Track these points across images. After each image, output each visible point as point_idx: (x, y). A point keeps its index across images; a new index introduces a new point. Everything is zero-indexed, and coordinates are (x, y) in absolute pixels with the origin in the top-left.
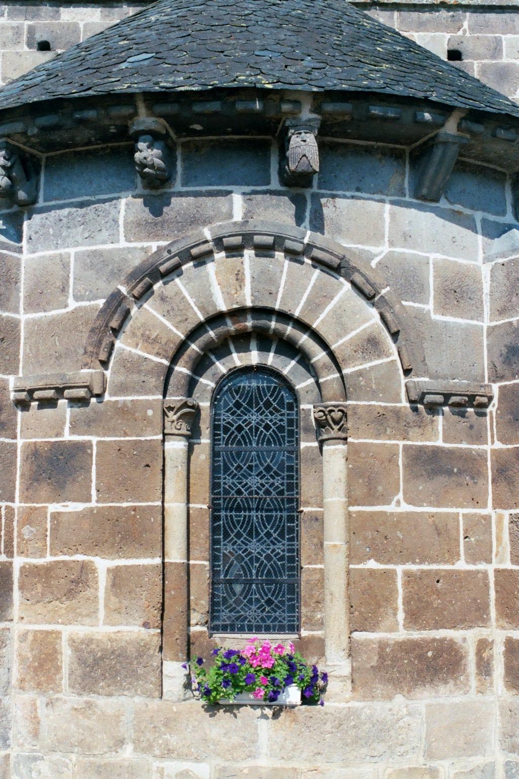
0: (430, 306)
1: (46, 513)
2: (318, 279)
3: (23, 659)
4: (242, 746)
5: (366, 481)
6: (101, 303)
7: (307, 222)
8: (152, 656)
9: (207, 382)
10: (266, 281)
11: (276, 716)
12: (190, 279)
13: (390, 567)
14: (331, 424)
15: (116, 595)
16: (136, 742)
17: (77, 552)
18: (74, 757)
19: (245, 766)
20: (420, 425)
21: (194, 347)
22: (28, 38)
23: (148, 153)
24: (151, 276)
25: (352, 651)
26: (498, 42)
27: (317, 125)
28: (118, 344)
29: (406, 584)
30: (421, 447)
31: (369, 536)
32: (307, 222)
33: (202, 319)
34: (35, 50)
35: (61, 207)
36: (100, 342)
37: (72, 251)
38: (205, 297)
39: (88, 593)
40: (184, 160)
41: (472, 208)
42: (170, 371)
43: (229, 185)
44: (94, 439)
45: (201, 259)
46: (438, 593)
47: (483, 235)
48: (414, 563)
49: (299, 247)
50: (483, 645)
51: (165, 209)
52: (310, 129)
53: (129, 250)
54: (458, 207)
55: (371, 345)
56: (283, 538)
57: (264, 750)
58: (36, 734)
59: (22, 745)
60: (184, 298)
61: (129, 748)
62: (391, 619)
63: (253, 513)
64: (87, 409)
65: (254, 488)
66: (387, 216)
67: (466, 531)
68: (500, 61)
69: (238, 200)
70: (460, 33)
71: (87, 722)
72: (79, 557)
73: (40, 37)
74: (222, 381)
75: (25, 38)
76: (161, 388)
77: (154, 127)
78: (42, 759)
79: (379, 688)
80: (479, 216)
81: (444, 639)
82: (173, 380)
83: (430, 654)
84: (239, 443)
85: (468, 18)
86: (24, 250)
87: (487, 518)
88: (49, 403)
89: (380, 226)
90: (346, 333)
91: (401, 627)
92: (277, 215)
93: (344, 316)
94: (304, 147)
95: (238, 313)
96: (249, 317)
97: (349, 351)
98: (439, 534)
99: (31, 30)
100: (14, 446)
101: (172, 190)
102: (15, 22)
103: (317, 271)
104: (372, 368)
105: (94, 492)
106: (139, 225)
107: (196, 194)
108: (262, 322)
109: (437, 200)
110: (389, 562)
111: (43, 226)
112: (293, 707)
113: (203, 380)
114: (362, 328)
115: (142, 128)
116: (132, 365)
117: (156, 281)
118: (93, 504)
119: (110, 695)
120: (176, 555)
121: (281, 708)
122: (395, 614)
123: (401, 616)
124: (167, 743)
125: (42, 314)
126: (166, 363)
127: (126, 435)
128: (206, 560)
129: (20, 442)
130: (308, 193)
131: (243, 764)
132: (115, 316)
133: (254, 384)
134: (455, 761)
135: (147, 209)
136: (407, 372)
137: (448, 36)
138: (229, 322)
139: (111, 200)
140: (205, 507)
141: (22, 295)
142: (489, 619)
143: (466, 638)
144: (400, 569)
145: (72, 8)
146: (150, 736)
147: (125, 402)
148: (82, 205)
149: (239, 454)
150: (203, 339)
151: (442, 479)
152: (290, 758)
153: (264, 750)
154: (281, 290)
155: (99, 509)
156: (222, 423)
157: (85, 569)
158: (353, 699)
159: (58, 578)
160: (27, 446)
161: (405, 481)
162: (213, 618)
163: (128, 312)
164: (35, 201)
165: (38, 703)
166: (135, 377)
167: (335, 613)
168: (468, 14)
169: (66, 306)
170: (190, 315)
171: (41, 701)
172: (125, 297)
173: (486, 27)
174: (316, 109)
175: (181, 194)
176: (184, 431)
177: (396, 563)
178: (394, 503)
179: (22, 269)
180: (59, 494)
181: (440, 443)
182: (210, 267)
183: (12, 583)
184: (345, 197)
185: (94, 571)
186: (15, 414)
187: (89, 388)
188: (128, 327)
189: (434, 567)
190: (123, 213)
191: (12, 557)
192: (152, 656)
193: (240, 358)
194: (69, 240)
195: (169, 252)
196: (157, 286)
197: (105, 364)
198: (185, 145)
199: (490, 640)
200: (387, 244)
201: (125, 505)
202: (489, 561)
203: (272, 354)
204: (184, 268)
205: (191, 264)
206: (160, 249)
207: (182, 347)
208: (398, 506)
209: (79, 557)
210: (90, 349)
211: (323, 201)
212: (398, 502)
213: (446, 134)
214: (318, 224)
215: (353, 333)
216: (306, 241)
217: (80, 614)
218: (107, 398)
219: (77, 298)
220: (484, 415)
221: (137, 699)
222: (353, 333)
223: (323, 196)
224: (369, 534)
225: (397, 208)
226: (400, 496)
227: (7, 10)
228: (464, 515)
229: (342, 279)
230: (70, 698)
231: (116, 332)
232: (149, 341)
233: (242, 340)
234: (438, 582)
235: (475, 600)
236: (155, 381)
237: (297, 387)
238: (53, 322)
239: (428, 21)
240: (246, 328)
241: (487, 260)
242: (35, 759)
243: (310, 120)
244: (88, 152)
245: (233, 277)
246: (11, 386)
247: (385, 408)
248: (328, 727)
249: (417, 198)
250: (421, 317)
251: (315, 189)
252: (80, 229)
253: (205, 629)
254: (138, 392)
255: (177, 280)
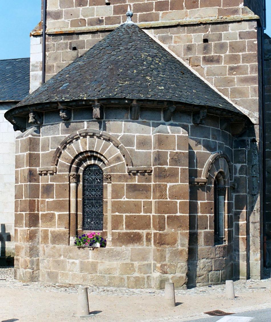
0: (135, 148)
1: (45, 201)
2: (105, 143)
3: (42, 236)
4: (85, 256)
5: (116, 193)
6: (55, 149)
7: (102, 129)
8: (67, 235)
9: (82, 168)
10: (92, 144)
11: (93, 249)
12: (75, 144)
13: (122, 214)
14: (109, 178)
15: (59, 221)
16: (64, 255)
17: (51, 211)
18: (51, 259)
19: (86, 261)
20: (131, 178)
21: (77, 160)
22: (70, 46)
23: (62, 114)
24: (65, 144)
25: (113, 234)
26: (221, 34)
27: (99, 106)
28: (59, 160)
29: (126, 219)
30: (131, 184)
31: (118, 207)
32: (102, 129)
33: (77, 154)
34: (72, 50)
35: (47, 125)
36: (55, 160)
37: (50, 136)
38: (78, 148)
39: (54, 220)
40: (73, 113)
41: (149, 120)
42: (71, 167)
43: (83, 119)
44: (55, 183)
45: (77, 139)
46: (135, 221)
47: (153, 127)
48: (128, 213)
49: (99, 135)
50: (148, 234)
51: (69, 126)
52: (98, 107)
53: (62, 137)
54: (144, 120)
55: (118, 159)
56: (100, 207)
57: (91, 257)
58: (44, 254)
59: (42, 257)
60: (73, 149)
61: (62, 256)
62: (122, 227)
63: (93, 201)
64: (53, 176)
65: (94, 195)
66: (123, 125)
67: (144, 205)
68: (221, 42)
69: (85, 123)
70: (208, 33)
71: (54, 251)
72: (52, 212)
73: (73, 46)
74: (85, 168)
75: (69, 46)
76: (68, 171)
77: (62, 108)
78: (45, 259)
79: (118, 244)
80: (151, 122)
81: (136, 232)
82: (72, 168)
83: (132, 236)
84: (90, 183)
85: (210, 27)
86: (41, 136)
87: (151, 201)
88: (46, 174)
89: (122, 128)
90: (112, 156)
91: (124, 229)
92: (95, 127)
93: (110, 152)
94: (97, 111)
95: (86, 152)
96: (89, 153)
97: (112, 161)
98: (135, 206)
99: (70, 43)
100: (39, 185)
101: (71, 121)
102: (66, 41)
103: (104, 141)
104: (118, 164)
105: (55, 196)
106: (64, 130)
107: (76, 122)
108: (92, 154)
109: (138, 119)
110: (121, 213)
111: (44, 130)
112: (97, 248)
113: (81, 168)
114: (116, 154)
115: (60, 108)
116: (62, 165)
117: (67, 144)
118: (55, 199)
119: (58, 244)
120: (73, 211)
121: (95, 248)
122: (123, 226)
123: (124, 226)
124: (70, 256)
125: (44, 152)
126: (69, 165)
127: (61, 182)
128: (81, 212)
129: (40, 184)
130: (102, 120)
131: (86, 260)
132: (58, 153)
133: (93, 168)
134: (139, 262)
135: (65, 126)
136: (127, 165)
137: (203, 34)
138: (84, 154)
139: (58, 124)
140: (81, 199)
141: (40, 147)
142: (150, 227)
143: (144, 232)
144: (124, 215)
145: (83, 35)
146: (66, 254)
147: (61, 174)
148: (52, 125)
149: (90, 186)
150: (78, 158)
151: (136, 192)
152: (96, 259)
153: (91, 257)
154: (95, 146)
155: (56, 200)
156: (86, 178)
157: (53, 215)
158: (111, 246)
159: (48, 217)
160: (42, 185)
161: (126, 193)
162: (83, 227)
163: (61, 153)
164: (42, 123)
165: (45, 247)
166: (63, 168)
167: (109, 225)
168: (210, 26)
169: (49, 150)
170: (75, 153)
171: (45, 246)
172: (60, 149)
173: (217, 30)
174: (98, 102)
175: (73, 122)
176: (75, 181)
177: (124, 213)
178: (123, 198)
179: (40, 140)
180: (48, 198)
181: (137, 183)
182: (79, 141)
183: (39, 218)
184: (112, 121)
185: (55, 215)
186: (39, 177)
187: (53, 171)
188: (61, 156)
189: (134, 214)
190: (60, 127)
191: (39, 212)
192: (67, 235)
193: (89, 162)
194: (49, 134)
195: (69, 138)
196: (68, 146)
197: (56, 165)
198: (73, 110)
199: (150, 233)
200: (123, 132)
201: (61, 199)
202: (151, 213)
203: (97, 161)
204: (73, 141)
205: (75, 140)
206: (69, 137)
207: (73, 161)
208: (124, 199)
209: (52, 212)
210: (53, 161)
211: (106, 122)
212: (124, 198)
213: (134, 105)
214: (105, 129)
215: (113, 156)
216: (101, 134)
217: (52, 226)
218: (57, 173)
219: (51, 148)
220: (151, 175)
221: (64, 245)
222: (113, 156)
223: (106, 121)
224: (116, 206)
225: (126, 123)
226: (125, 197)
227: (63, 38)
228: (143, 201)
229: (111, 142)
230: (50, 245)
231: (59, 157)
232: (66, 159)
233: (90, 158)
234: (135, 218)
235: (146, 223)
236: (67, 169)
237: (103, 169)
238: (47, 154)
239: (197, 29)
240: (89, 155)
241: (153, 134)
242: (44, 259)
243: (97, 105)
244: (53, 111)
245: (84, 143)
246: (38, 170)
247: (121, 174)
248: (105, 252)
249: (132, 119)
250: (131, 151)
251: (104, 120)
252: (52, 131)
253: (81, 229)
254: (64, 172)
255: (72, 144)
